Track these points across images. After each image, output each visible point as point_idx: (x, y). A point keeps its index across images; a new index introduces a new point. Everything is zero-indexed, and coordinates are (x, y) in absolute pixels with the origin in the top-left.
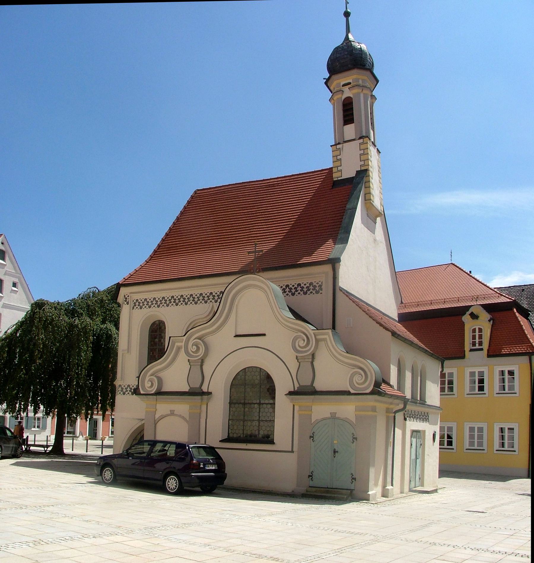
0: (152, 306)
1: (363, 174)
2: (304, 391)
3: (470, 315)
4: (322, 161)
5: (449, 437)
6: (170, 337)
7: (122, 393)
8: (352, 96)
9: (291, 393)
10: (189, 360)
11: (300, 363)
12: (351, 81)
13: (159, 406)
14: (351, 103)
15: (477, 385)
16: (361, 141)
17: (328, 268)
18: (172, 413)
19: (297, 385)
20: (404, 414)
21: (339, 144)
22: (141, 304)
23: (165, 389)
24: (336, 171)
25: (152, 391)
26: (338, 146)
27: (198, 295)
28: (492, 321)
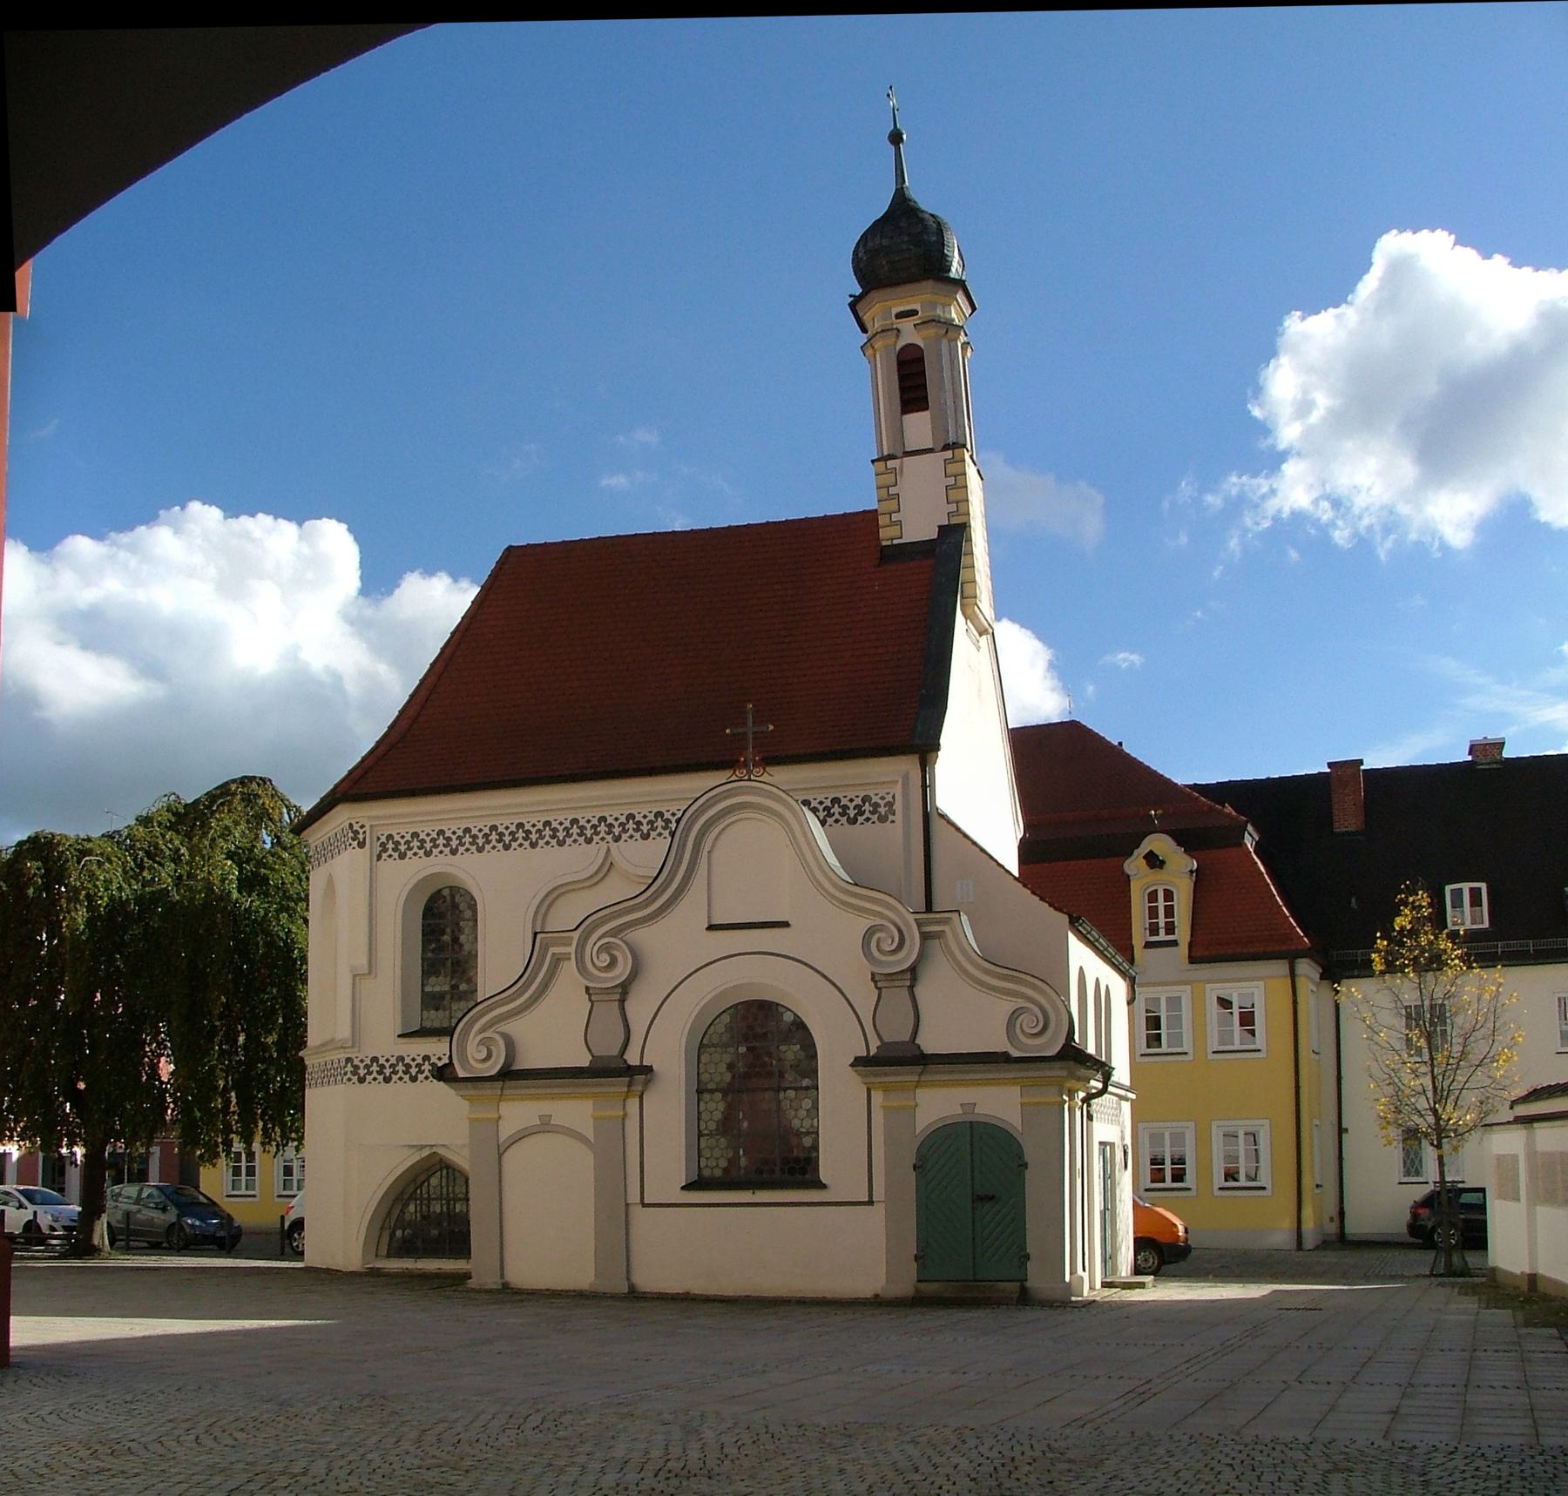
1: (955, 535)
2: (895, 1060)
4: (850, 492)
6: (535, 934)
9: (858, 1062)
10: (587, 988)
12: (917, 306)
13: (507, 1108)
14: (921, 360)
16: (949, 454)
18: (545, 1126)
19: (874, 1044)
21: (891, 457)
23: (523, 1063)
25: (489, 1069)
26: (890, 464)
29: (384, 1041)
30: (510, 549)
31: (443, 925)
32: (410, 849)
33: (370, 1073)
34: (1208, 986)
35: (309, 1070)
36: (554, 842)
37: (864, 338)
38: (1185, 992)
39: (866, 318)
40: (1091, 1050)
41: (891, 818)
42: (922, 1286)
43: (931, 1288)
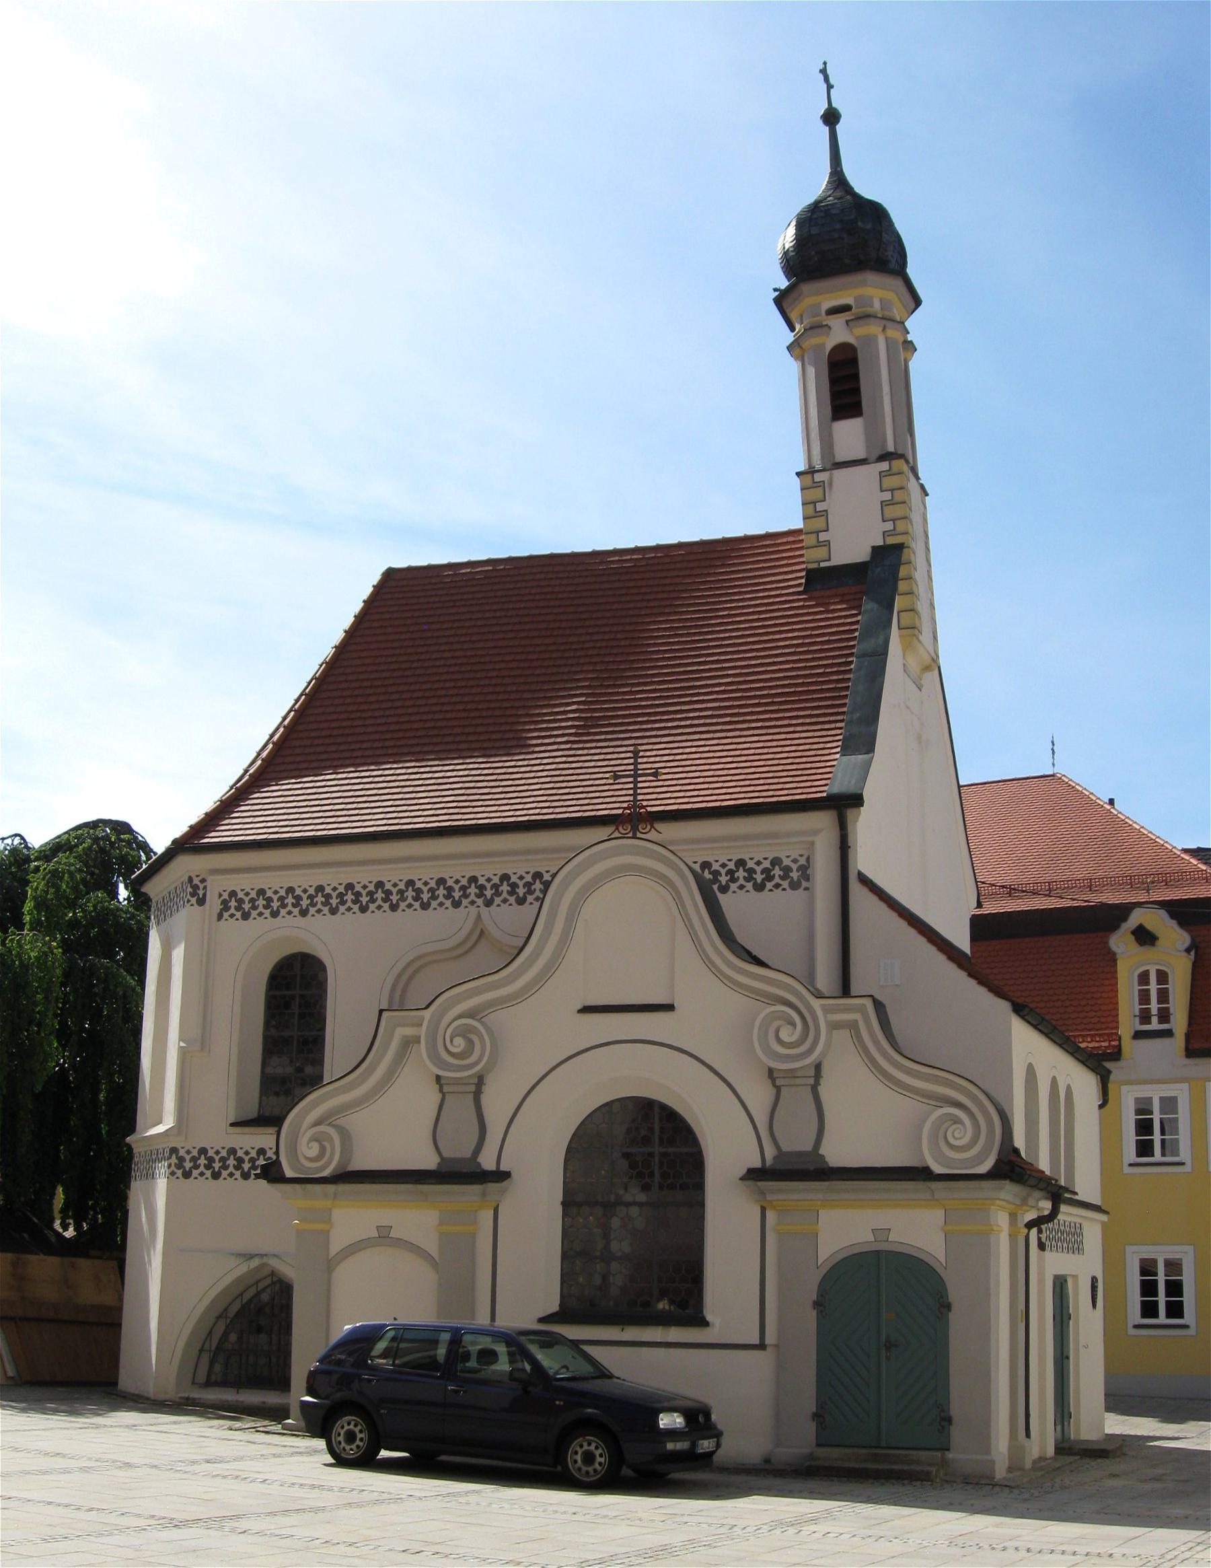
3: (1134, 932)
6: (381, 1011)
8: (852, 341)
9: (754, 1175)
11: (778, 1089)
12: (849, 300)
15: (1157, 1137)
16: (884, 466)
17: (823, 821)
19: (770, 1153)
26: (819, 477)
28: (1193, 953)
29: (217, 1135)
31: (294, 1001)
35: (136, 1159)
37: (790, 337)
38: (1181, 1091)
39: (793, 316)
40: (1044, 1165)
41: (804, 884)
42: (821, 1452)
43: (832, 1455)
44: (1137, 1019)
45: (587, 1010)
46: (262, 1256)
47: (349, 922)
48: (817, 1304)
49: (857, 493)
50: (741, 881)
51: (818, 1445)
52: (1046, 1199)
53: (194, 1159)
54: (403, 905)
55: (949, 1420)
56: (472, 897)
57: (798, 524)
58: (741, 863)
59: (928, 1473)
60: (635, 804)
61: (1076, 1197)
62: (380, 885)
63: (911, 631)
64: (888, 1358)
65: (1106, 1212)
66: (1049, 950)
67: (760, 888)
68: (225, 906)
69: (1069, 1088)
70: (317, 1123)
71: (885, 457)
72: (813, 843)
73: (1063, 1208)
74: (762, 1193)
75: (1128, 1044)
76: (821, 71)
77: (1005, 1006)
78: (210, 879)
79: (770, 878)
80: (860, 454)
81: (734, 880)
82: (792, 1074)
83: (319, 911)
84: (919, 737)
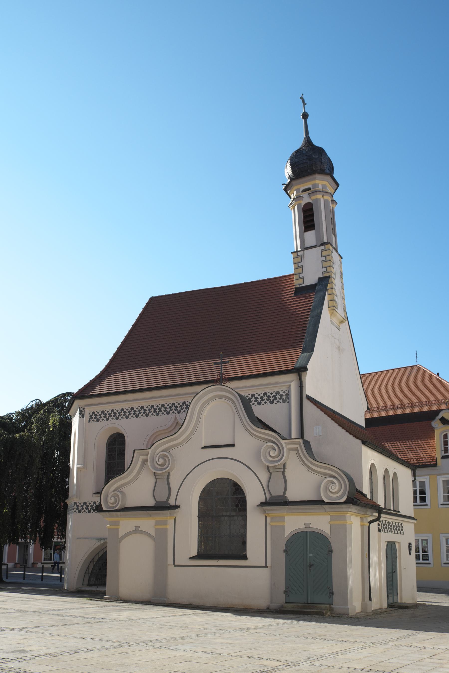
0: (110, 418)
1: (324, 281)
2: (276, 502)
3: (440, 420)
4: (282, 267)
5: (424, 551)
6: (134, 450)
7: (77, 511)
8: (310, 201)
9: (263, 504)
11: (271, 473)
12: (310, 186)
14: (312, 209)
16: (323, 247)
19: (268, 497)
20: (379, 525)
22: (98, 417)
24: (298, 278)
26: (299, 253)
27: (160, 406)
30: (152, 299)
32: (101, 417)
33: (83, 509)
34: (438, 477)
36: (155, 414)
41: (288, 400)
43: (289, 606)
44: (443, 452)
45: (205, 447)
46: (105, 539)
47: (133, 420)
48: (285, 551)
49: (313, 258)
50: (265, 400)
51: (286, 603)
52: (376, 512)
53: (82, 506)
54: (150, 414)
55: (332, 593)
56: (173, 410)
57: (293, 272)
58: (265, 394)
59: (322, 612)
60: (221, 374)
61: (400, 513)
62: (142, 407)
63: (333, 308)
64: (310, 570)
65: (416, 520)
66: (399, 424)
67: (272, 402)
68: (91, 417)
69: (395, 474)
70: (114, 491)
71: (324, 244)
72: (290, 385)
73: (382, 515)
74: (265, 511)
75: (439, 461)
76: (306, 104)
77: (359, 442)
78: (85, 408)
79: (275, 399)
80: (314, 244)
81: (263, 400)
82: (275, 468)
83: (122, 418)
84: (339, 348)
